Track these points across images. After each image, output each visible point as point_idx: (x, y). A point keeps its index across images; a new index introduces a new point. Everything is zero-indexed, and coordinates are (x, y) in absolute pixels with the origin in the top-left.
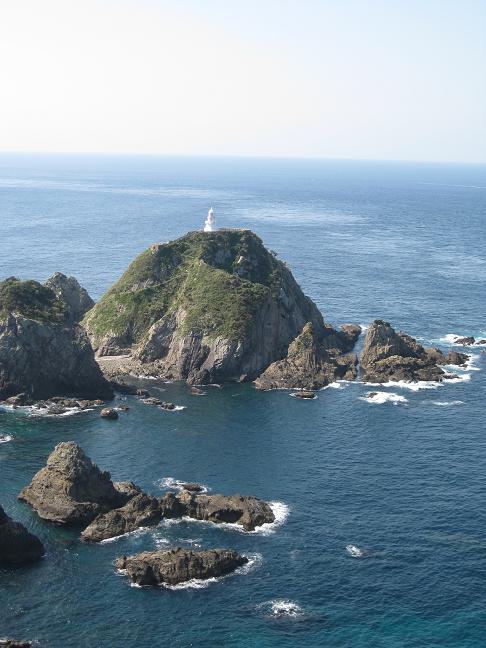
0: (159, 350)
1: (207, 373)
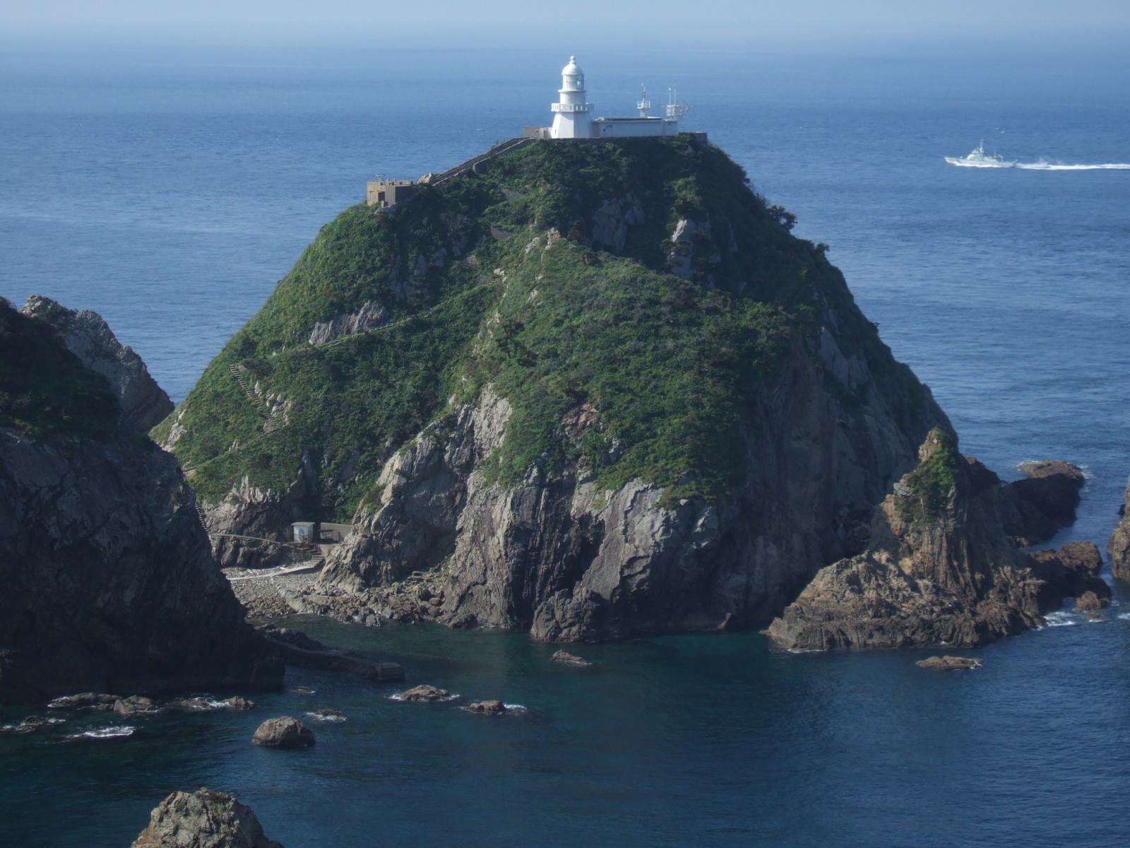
0: (418, 538)
1: (600, 607)
